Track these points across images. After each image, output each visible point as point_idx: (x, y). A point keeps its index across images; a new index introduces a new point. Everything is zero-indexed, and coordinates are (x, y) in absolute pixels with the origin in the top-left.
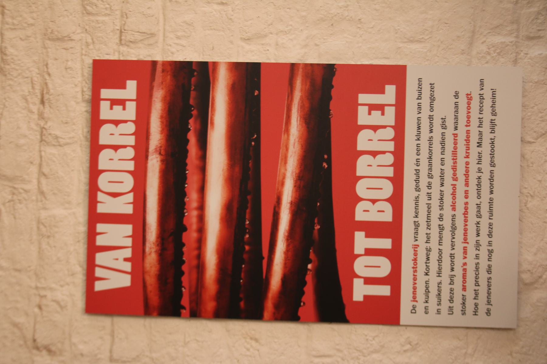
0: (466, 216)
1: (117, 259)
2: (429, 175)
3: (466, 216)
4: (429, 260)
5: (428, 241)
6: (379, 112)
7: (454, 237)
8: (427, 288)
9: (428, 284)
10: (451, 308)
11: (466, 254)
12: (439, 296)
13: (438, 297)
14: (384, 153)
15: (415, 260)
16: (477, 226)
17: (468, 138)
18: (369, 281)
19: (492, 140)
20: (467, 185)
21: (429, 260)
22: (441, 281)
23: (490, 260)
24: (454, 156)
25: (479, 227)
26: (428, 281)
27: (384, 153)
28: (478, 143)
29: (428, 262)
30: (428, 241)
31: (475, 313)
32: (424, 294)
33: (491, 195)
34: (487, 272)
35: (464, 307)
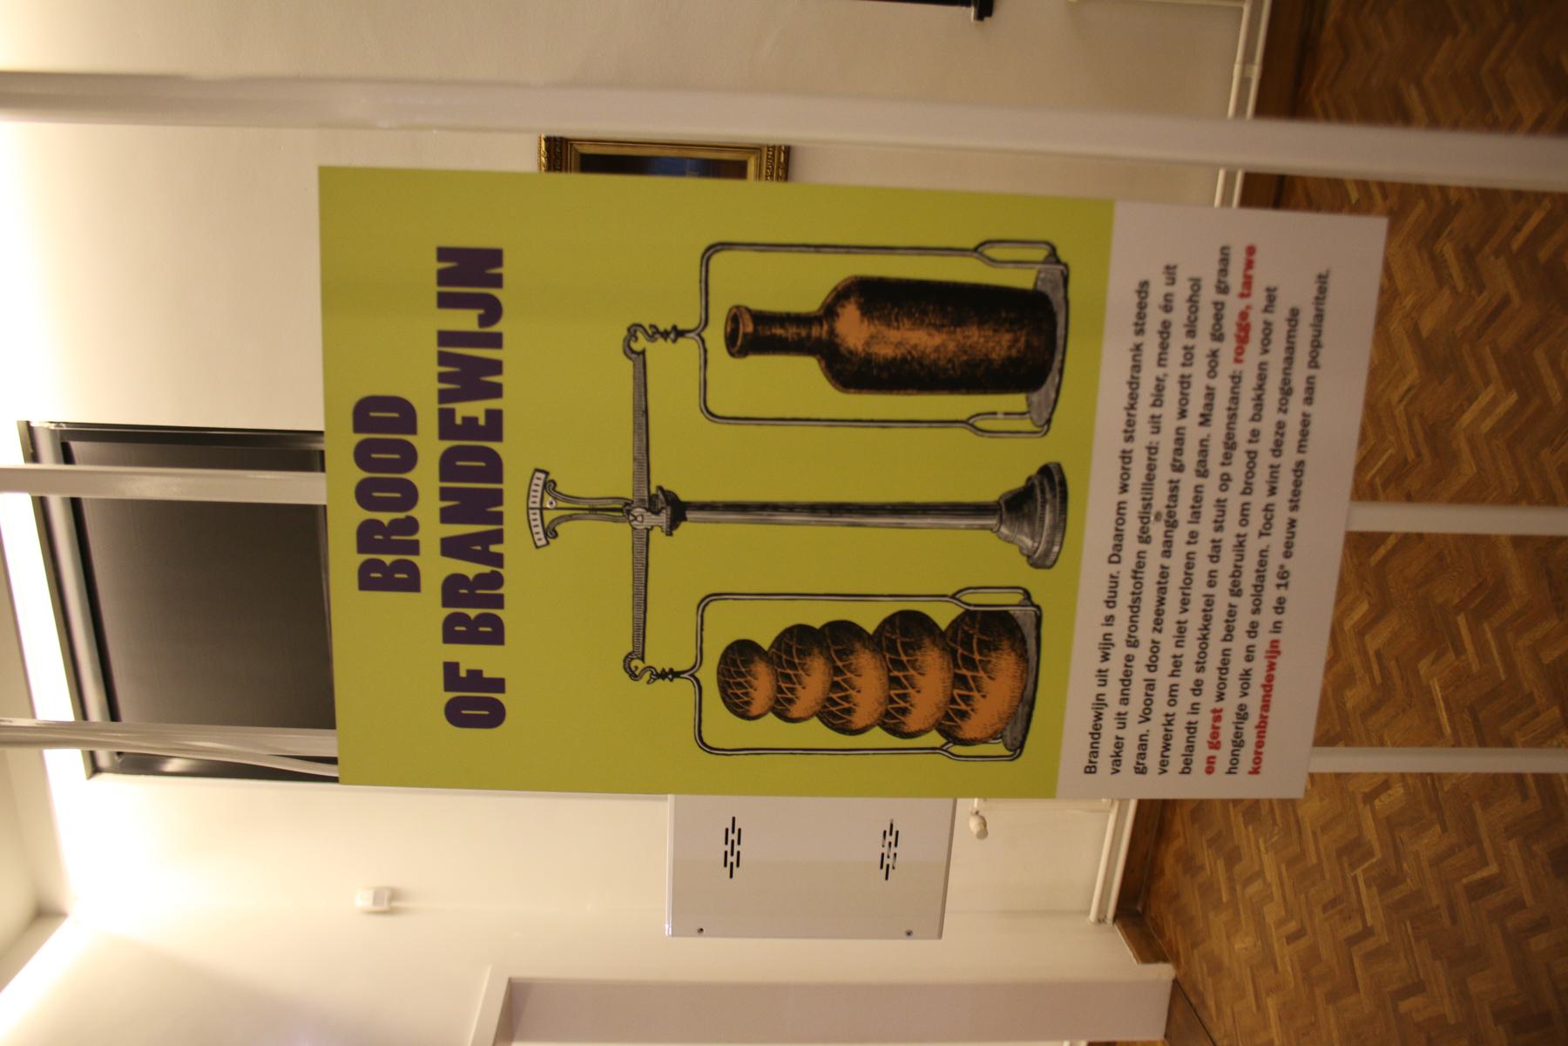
2: (1129, 639)
7: (1246, 691)
8: (1229, 631)
9: (1176, 696)
12: (1241, 548)
13: (1238, 551)
16: (1166, 730)
19: (1169, 718)
20: (1167, 553)
23: (1180, 644)
24: (1147, 494)
25: (1171, 731)
26: (1146, 735)
31: (1186, 769)
32: (1267, 482)
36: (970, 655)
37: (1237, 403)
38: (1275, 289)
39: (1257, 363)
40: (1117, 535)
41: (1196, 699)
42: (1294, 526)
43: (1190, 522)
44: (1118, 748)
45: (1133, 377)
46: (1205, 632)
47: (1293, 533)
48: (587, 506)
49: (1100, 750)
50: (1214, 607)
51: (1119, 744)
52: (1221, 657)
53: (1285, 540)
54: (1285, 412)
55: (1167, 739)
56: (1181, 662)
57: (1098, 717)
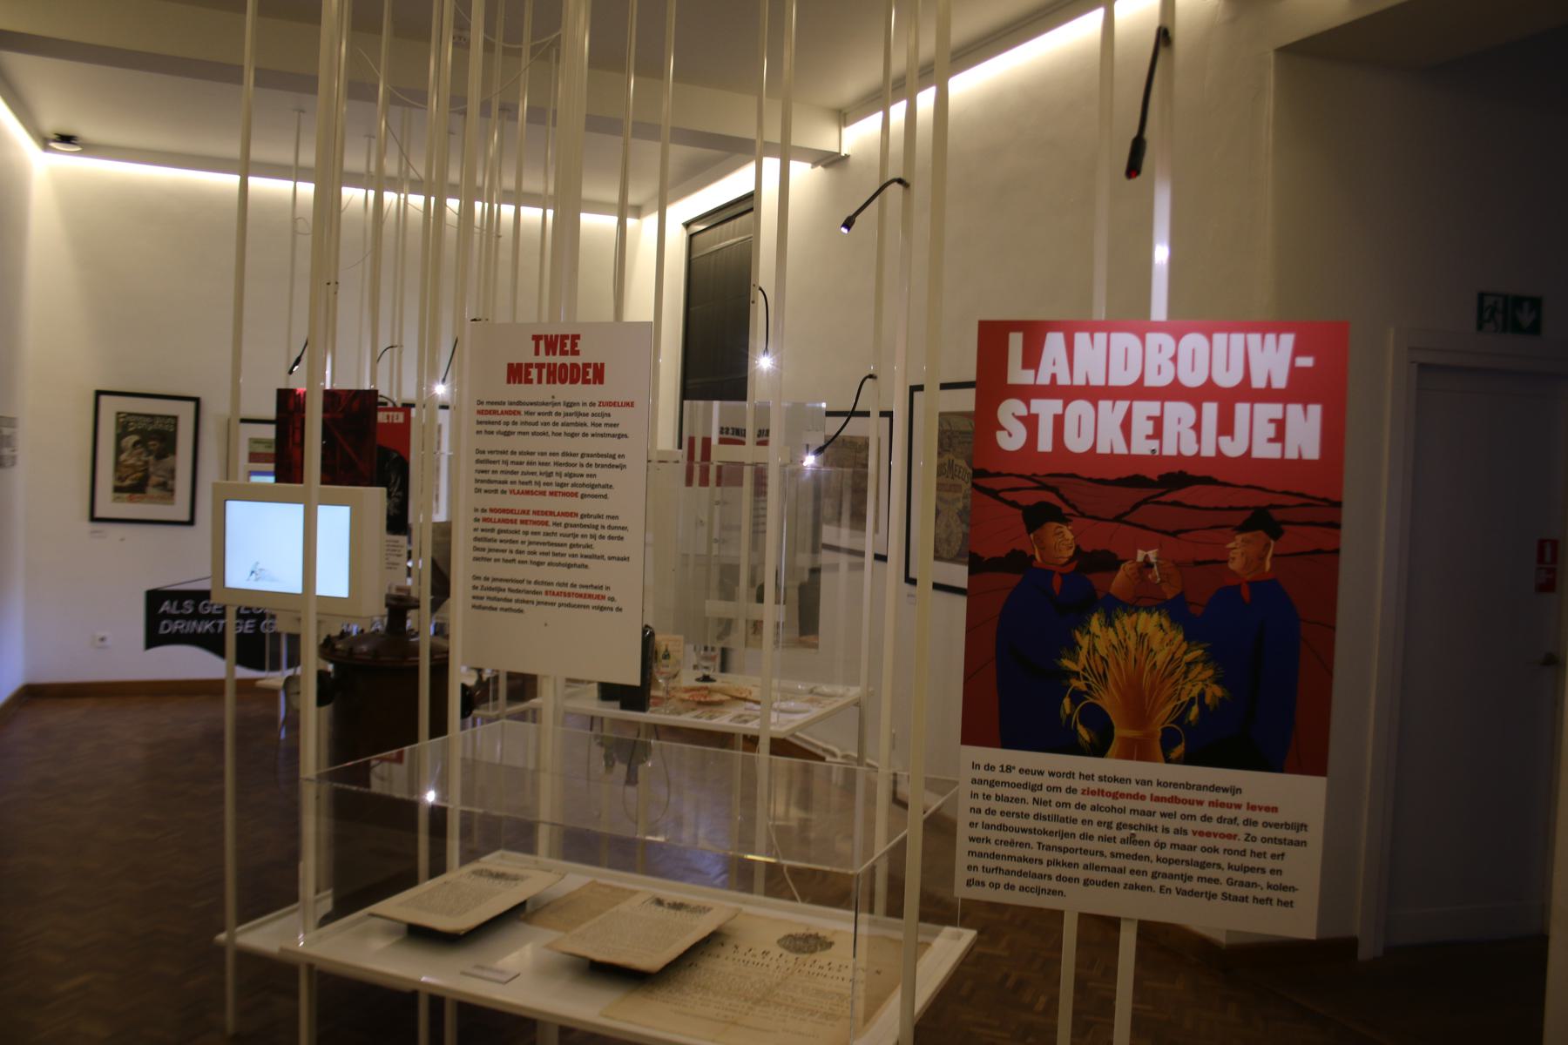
1: (1054, 364)
6: (1150, 432)
10: (976, 868)
14: (1199, 441)
17: (1092, 792)
18: (1059, 421)
27: (1199, 441)
31: (971, 853)
36: (366, 790)
37: (1288, 844)
41: (1063, 790)
42: (1236, 807)
43: (1152, 795)
45: (1225, 819)
47: (1231, 807)
48: (749, 705)
51: (1204, 849)
52: (1126, 793)
53: (1030, 769)
57: (1225, 790)
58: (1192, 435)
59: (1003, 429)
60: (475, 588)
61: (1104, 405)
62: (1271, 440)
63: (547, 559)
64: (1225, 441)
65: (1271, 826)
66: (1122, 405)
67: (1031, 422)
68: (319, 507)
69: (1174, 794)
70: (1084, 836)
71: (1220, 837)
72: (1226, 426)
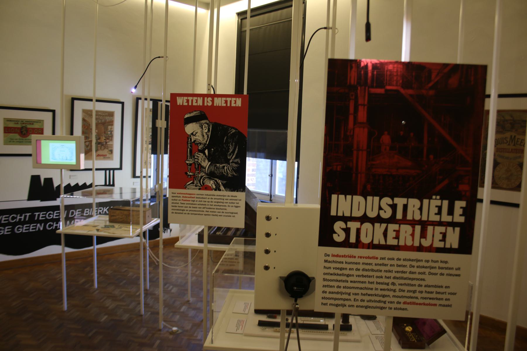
0: (362, 276)
3: (362, 276)
4: (331, 275)
5: (325, 268)
9: (352, 270)
11: (390, 303)
15: (220, 196)
18: (358, 231)
21: (331, 275)
22: (408, 310)
26: (350, 300)
28: (327, 260)
29: (330, 274)
30: (325, 268)
31: (172, 206)
33: (355, 276)
34: (363, 268)
35: (408, 260)
38: (451, 307)
39: (354, 274)
40: (330, 261)
44: (339, 281)
46: (337, 274)
49: (333, 294)
50: (368, 278)
51: (419, 273)
54: (443, 299)
55: (433, 299)
56: (366, 277)
58: (411, 238)
59: (336, 233)
60: (326, 261)
61: (377, 225)
62: (436, 214)
63: (223, 214)
64: (423, 240)
65: (364, 258)
66: (384, 225)
67: (347, 231)
68: (218, 292)
69: (383, 262)
70: (411, 273)
71: (365, 258)
72: (423, 235)
